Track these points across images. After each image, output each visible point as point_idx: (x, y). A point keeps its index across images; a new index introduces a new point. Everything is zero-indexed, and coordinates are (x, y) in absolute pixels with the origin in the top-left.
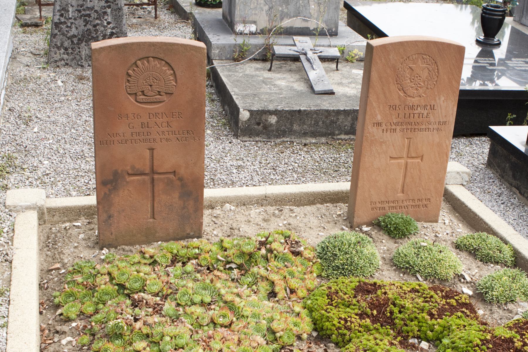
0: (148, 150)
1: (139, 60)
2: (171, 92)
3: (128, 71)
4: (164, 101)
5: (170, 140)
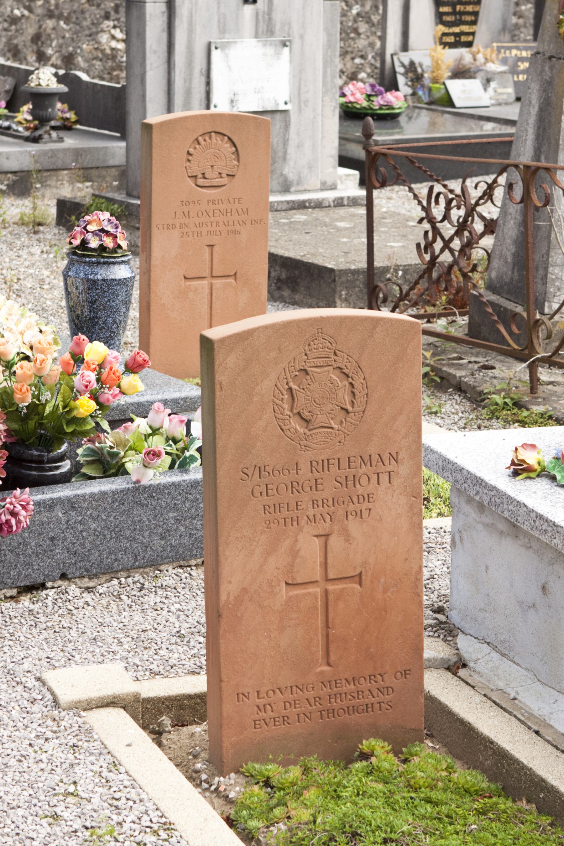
4: (225, 185)
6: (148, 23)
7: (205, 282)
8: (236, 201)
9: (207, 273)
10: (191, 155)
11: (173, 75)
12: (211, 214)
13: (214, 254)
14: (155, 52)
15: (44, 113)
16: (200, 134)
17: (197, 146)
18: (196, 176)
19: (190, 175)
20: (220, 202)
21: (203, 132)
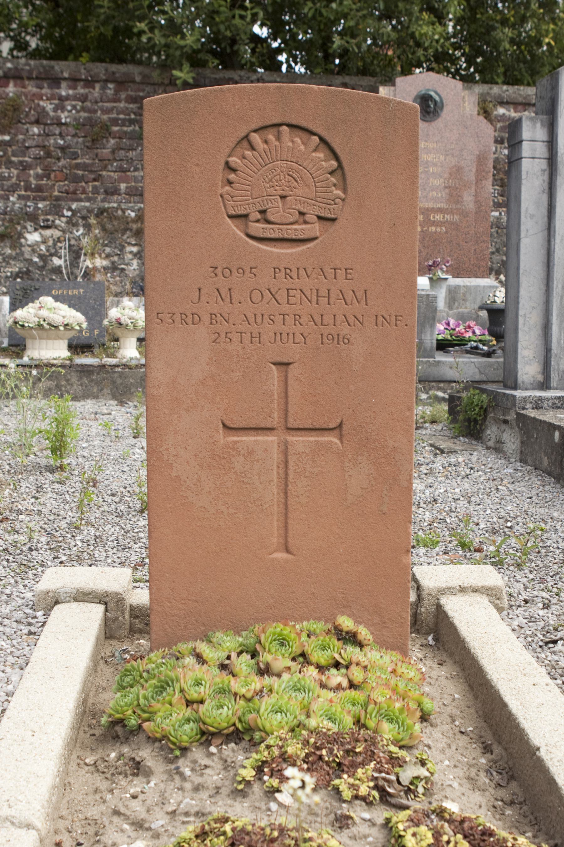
0: (273, 367)
1: (255, 131)
2: (333, 216)
3: (231, 159)
4: (315, 239)
5: (346, 341)
6: (524, 182)
7: (271, 438)
8: (341, 274)
9: (275, 419)
10: (234, 170)
11: (552, 243)
12: (282, 296)
13: (291, 382)
14: (532, 216)
15: (499, 329)
16: (254, 127)
17: (248, 153)
18: (246, 216)
19: (232, 212)
20: (302, 272)
21: (261, 124)
